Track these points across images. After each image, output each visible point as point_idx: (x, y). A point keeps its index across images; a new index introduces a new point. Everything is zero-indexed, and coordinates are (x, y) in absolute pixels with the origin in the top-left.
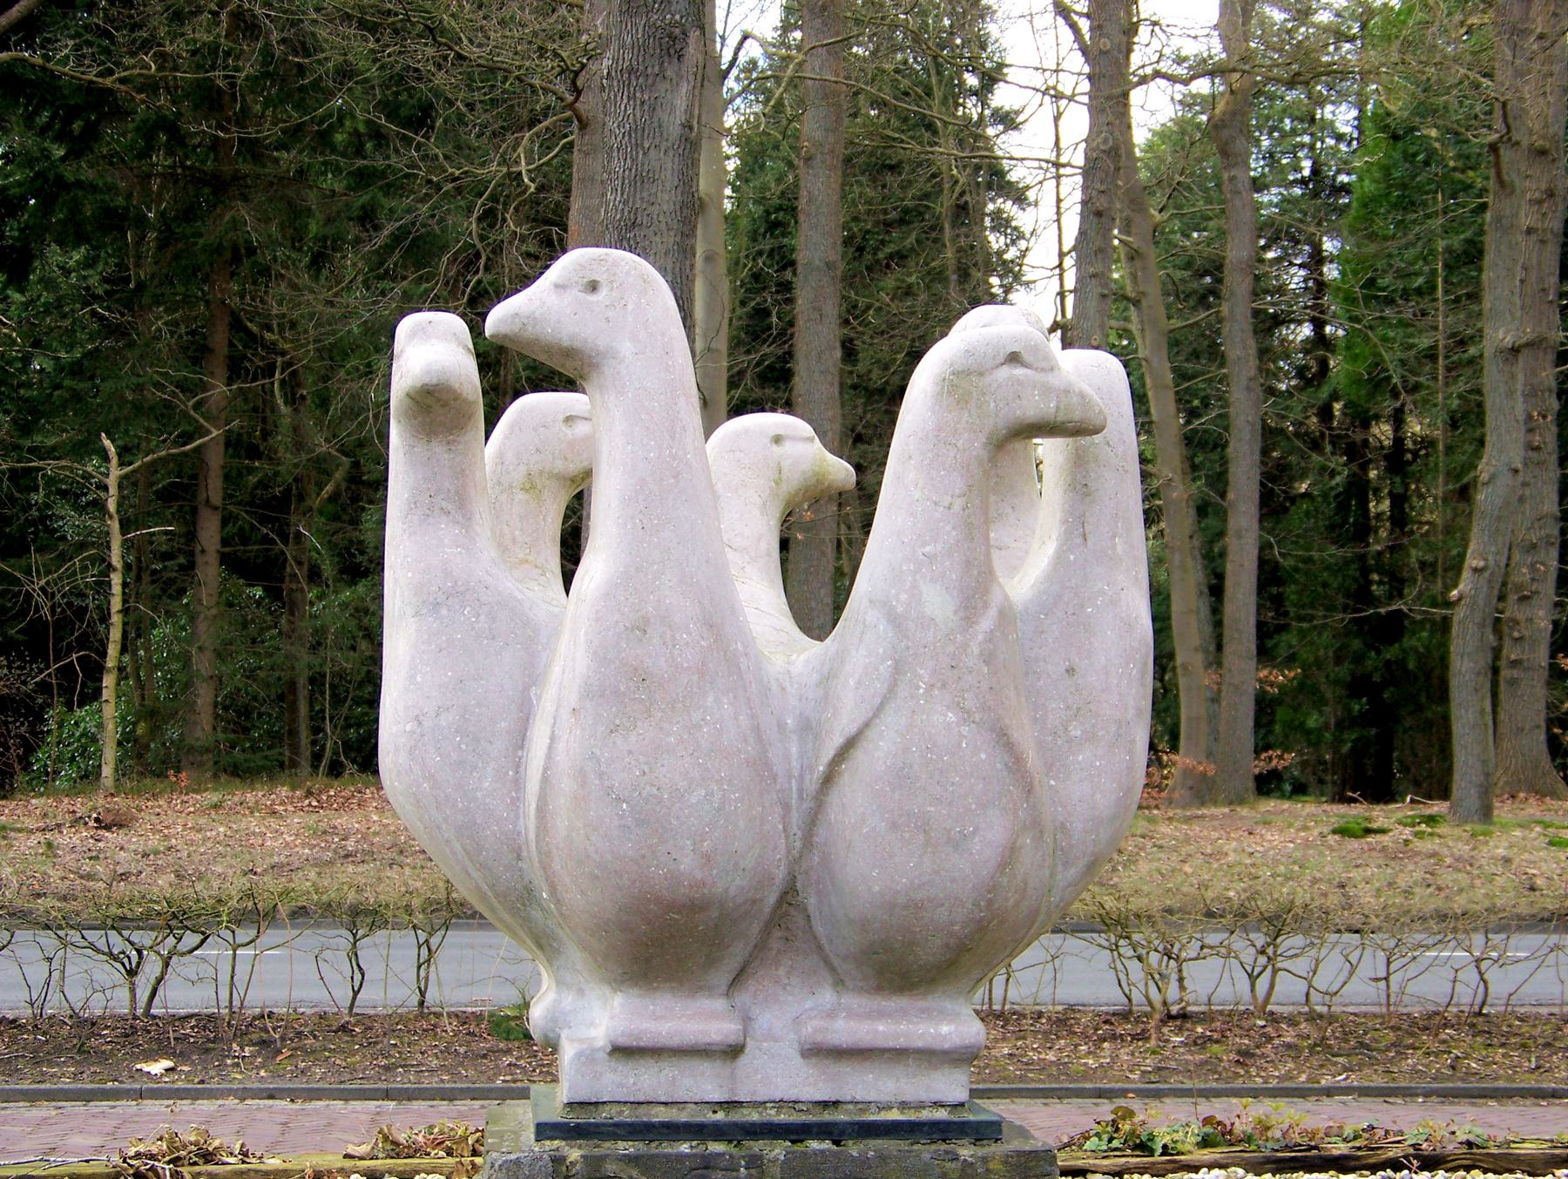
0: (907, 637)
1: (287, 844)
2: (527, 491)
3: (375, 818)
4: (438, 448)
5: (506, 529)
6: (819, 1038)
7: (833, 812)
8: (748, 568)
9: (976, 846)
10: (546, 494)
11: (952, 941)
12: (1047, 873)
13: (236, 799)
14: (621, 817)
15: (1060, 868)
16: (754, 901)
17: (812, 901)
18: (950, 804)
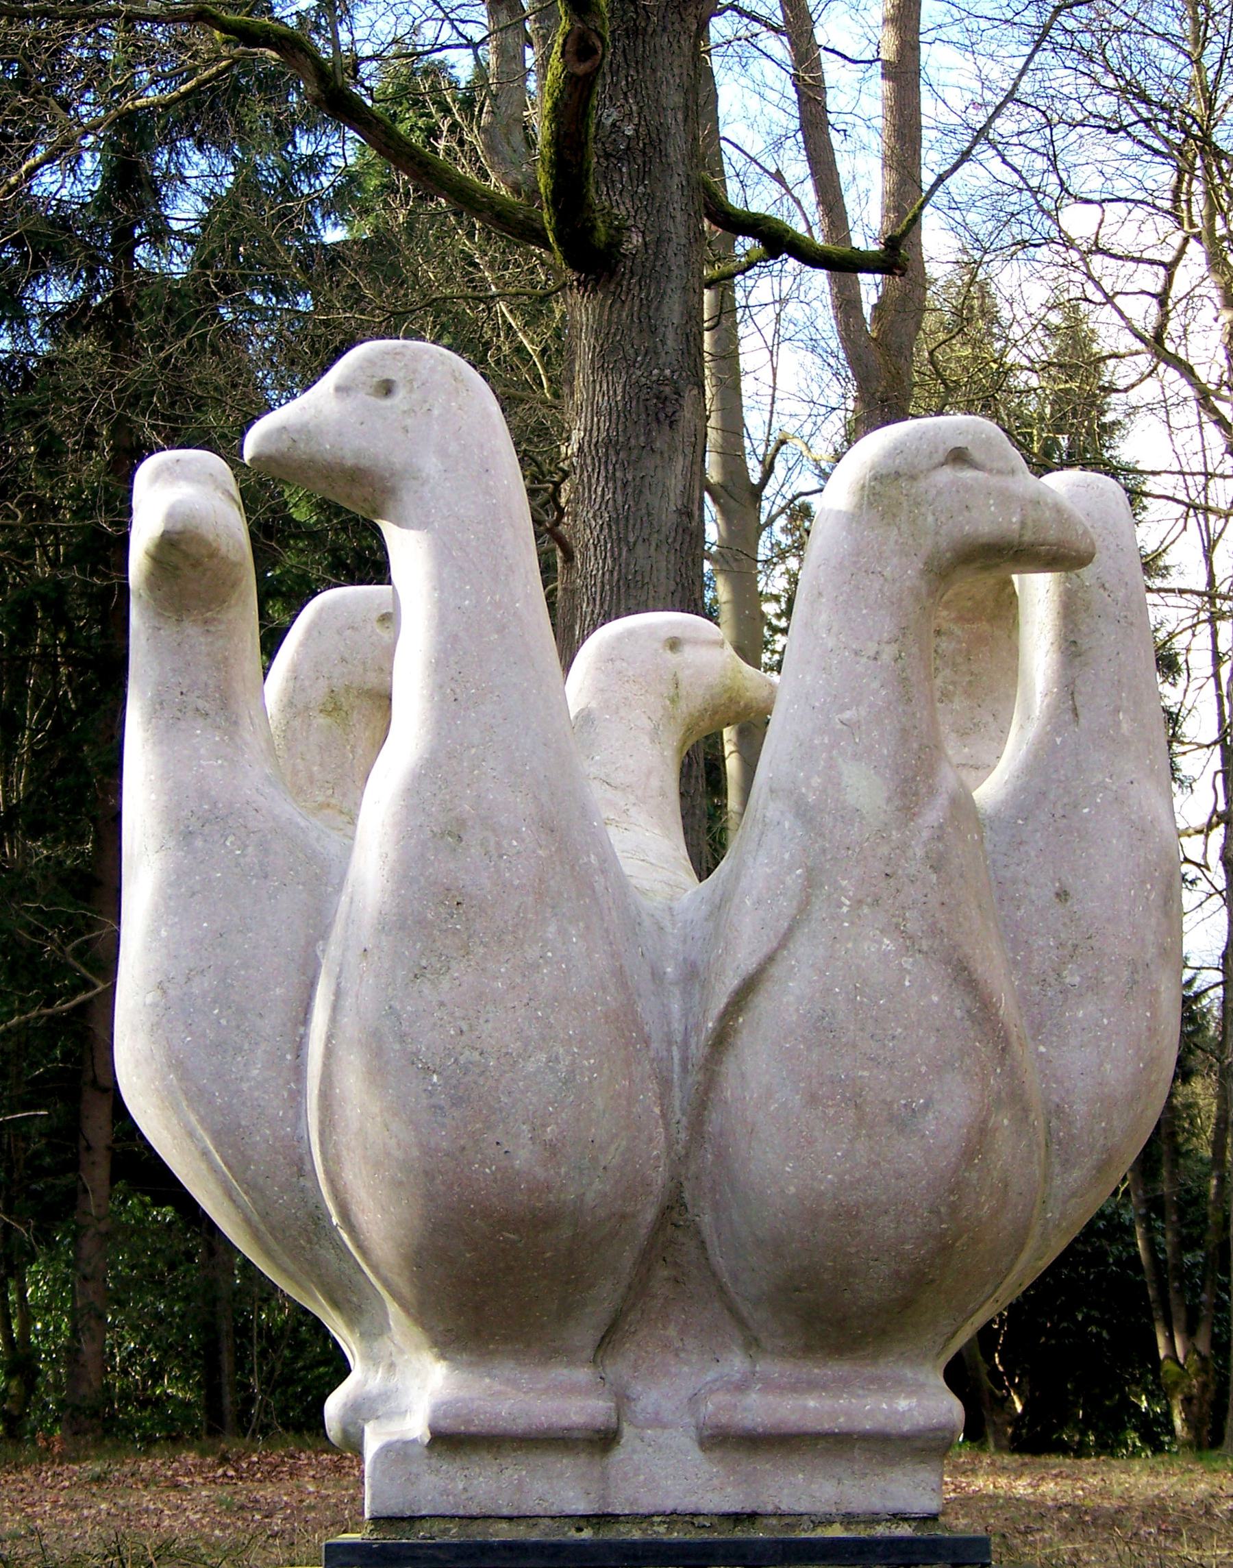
0: (822, 835)
1: (192, 1524)
2: (329, 713)
3: (311, 1489)
4: (192, 630)
5: (300, 765)
6: (724, 1419)
7: (729, 1088)
8: (633, 811)
9: (929, 1124)
10: (355, 715)
11: (904, 1268)
12: (1038, 1171)
13: (126, 1469)
14: (431, 1094)
15: (1057, 1169)
16: (623, 1217)
17: (706, 1220)
18: (891, 1066)
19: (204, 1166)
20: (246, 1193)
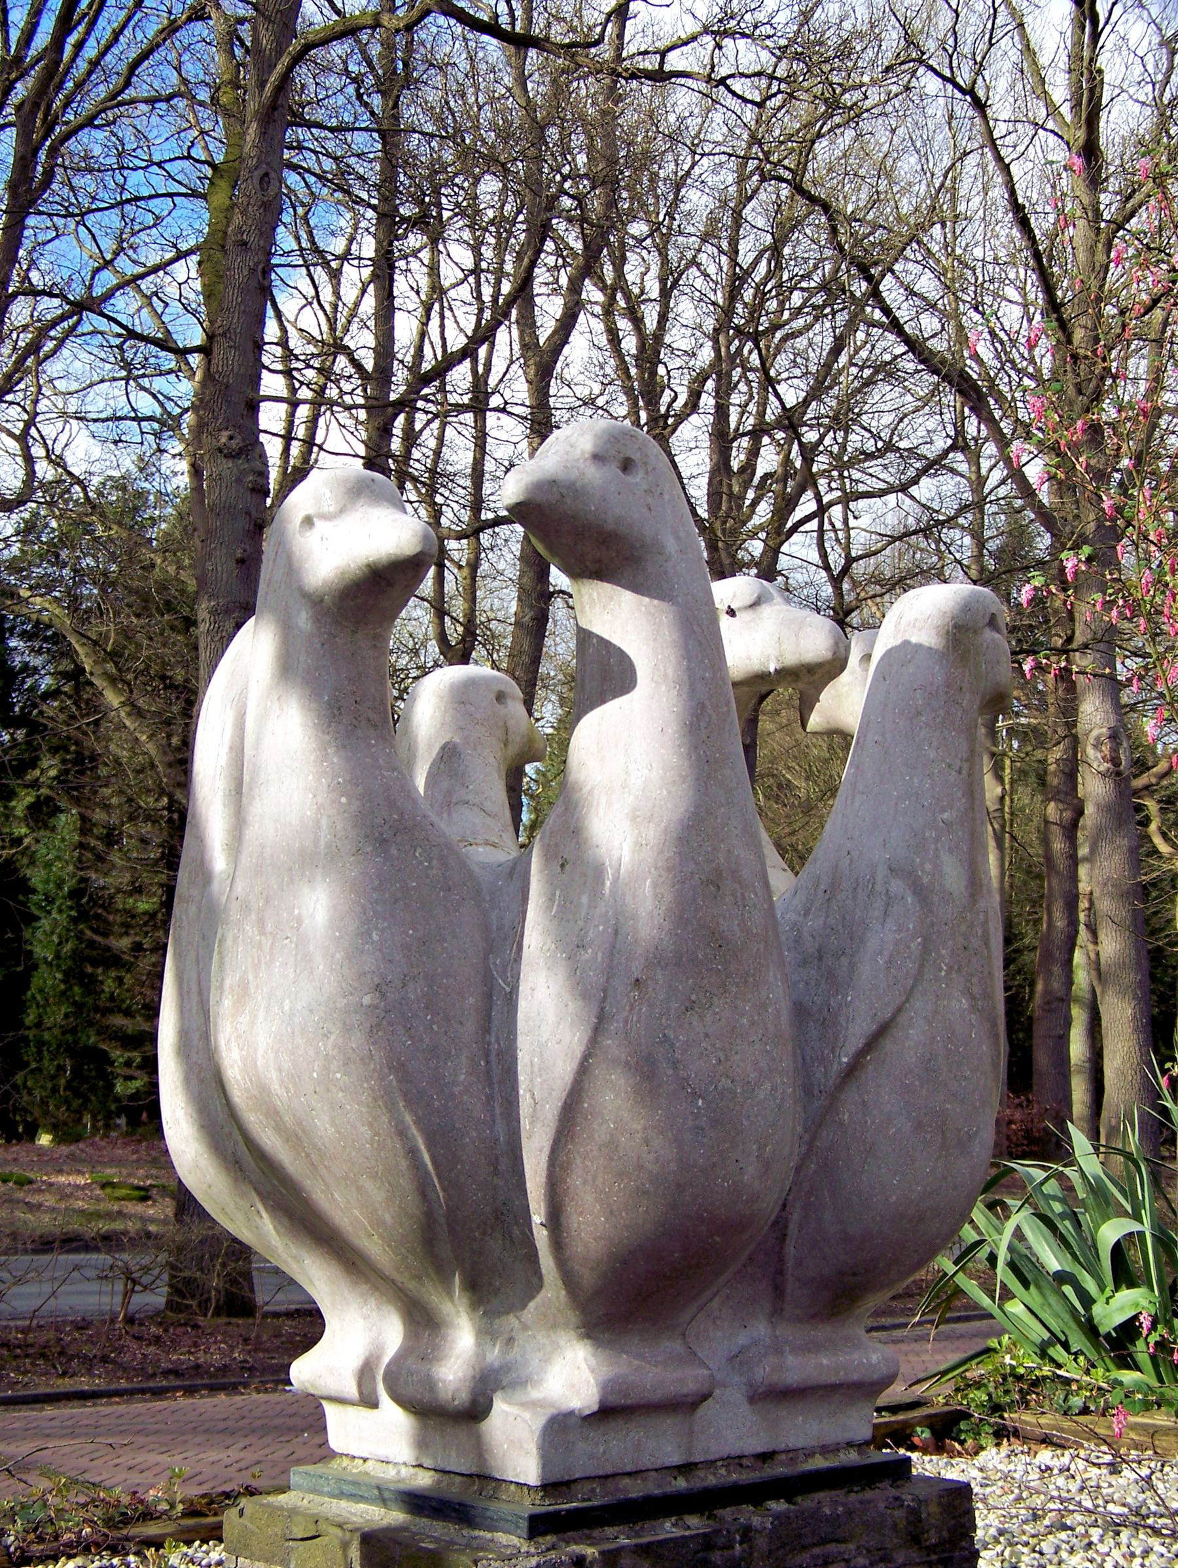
6: (775, 1378)
14: (696, 1117)
19: (404, 1164)
20: (444, 1190)
